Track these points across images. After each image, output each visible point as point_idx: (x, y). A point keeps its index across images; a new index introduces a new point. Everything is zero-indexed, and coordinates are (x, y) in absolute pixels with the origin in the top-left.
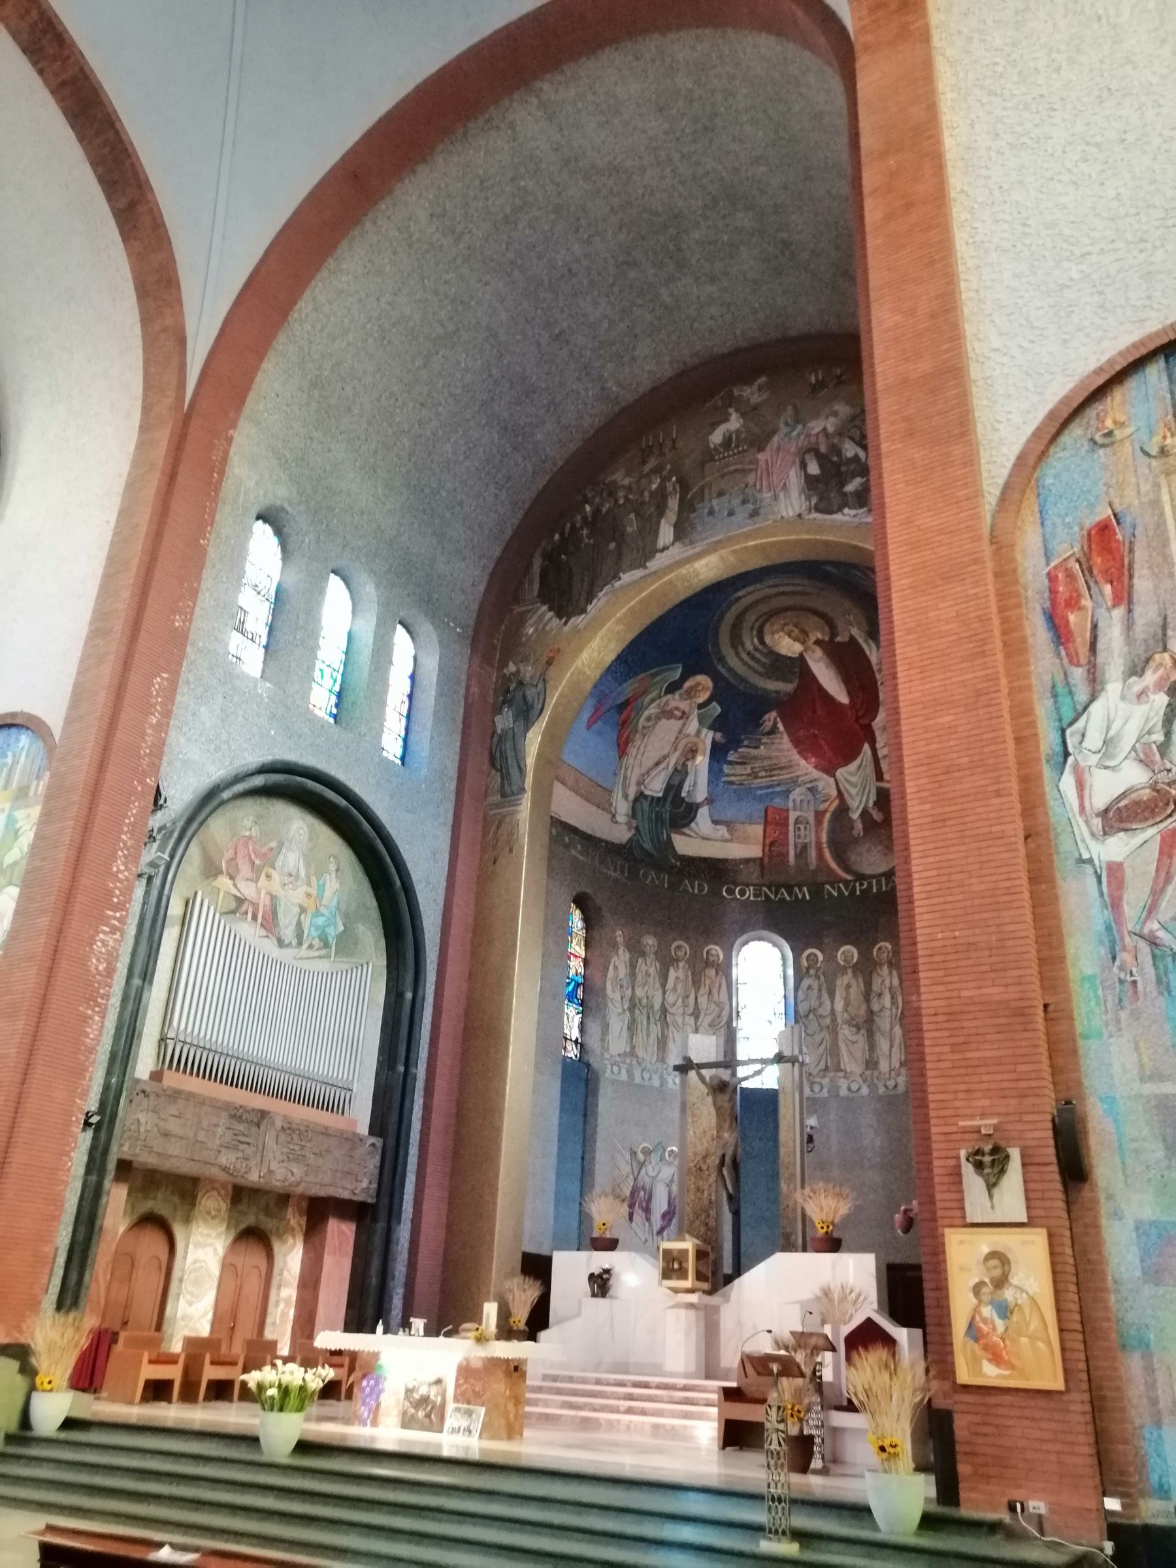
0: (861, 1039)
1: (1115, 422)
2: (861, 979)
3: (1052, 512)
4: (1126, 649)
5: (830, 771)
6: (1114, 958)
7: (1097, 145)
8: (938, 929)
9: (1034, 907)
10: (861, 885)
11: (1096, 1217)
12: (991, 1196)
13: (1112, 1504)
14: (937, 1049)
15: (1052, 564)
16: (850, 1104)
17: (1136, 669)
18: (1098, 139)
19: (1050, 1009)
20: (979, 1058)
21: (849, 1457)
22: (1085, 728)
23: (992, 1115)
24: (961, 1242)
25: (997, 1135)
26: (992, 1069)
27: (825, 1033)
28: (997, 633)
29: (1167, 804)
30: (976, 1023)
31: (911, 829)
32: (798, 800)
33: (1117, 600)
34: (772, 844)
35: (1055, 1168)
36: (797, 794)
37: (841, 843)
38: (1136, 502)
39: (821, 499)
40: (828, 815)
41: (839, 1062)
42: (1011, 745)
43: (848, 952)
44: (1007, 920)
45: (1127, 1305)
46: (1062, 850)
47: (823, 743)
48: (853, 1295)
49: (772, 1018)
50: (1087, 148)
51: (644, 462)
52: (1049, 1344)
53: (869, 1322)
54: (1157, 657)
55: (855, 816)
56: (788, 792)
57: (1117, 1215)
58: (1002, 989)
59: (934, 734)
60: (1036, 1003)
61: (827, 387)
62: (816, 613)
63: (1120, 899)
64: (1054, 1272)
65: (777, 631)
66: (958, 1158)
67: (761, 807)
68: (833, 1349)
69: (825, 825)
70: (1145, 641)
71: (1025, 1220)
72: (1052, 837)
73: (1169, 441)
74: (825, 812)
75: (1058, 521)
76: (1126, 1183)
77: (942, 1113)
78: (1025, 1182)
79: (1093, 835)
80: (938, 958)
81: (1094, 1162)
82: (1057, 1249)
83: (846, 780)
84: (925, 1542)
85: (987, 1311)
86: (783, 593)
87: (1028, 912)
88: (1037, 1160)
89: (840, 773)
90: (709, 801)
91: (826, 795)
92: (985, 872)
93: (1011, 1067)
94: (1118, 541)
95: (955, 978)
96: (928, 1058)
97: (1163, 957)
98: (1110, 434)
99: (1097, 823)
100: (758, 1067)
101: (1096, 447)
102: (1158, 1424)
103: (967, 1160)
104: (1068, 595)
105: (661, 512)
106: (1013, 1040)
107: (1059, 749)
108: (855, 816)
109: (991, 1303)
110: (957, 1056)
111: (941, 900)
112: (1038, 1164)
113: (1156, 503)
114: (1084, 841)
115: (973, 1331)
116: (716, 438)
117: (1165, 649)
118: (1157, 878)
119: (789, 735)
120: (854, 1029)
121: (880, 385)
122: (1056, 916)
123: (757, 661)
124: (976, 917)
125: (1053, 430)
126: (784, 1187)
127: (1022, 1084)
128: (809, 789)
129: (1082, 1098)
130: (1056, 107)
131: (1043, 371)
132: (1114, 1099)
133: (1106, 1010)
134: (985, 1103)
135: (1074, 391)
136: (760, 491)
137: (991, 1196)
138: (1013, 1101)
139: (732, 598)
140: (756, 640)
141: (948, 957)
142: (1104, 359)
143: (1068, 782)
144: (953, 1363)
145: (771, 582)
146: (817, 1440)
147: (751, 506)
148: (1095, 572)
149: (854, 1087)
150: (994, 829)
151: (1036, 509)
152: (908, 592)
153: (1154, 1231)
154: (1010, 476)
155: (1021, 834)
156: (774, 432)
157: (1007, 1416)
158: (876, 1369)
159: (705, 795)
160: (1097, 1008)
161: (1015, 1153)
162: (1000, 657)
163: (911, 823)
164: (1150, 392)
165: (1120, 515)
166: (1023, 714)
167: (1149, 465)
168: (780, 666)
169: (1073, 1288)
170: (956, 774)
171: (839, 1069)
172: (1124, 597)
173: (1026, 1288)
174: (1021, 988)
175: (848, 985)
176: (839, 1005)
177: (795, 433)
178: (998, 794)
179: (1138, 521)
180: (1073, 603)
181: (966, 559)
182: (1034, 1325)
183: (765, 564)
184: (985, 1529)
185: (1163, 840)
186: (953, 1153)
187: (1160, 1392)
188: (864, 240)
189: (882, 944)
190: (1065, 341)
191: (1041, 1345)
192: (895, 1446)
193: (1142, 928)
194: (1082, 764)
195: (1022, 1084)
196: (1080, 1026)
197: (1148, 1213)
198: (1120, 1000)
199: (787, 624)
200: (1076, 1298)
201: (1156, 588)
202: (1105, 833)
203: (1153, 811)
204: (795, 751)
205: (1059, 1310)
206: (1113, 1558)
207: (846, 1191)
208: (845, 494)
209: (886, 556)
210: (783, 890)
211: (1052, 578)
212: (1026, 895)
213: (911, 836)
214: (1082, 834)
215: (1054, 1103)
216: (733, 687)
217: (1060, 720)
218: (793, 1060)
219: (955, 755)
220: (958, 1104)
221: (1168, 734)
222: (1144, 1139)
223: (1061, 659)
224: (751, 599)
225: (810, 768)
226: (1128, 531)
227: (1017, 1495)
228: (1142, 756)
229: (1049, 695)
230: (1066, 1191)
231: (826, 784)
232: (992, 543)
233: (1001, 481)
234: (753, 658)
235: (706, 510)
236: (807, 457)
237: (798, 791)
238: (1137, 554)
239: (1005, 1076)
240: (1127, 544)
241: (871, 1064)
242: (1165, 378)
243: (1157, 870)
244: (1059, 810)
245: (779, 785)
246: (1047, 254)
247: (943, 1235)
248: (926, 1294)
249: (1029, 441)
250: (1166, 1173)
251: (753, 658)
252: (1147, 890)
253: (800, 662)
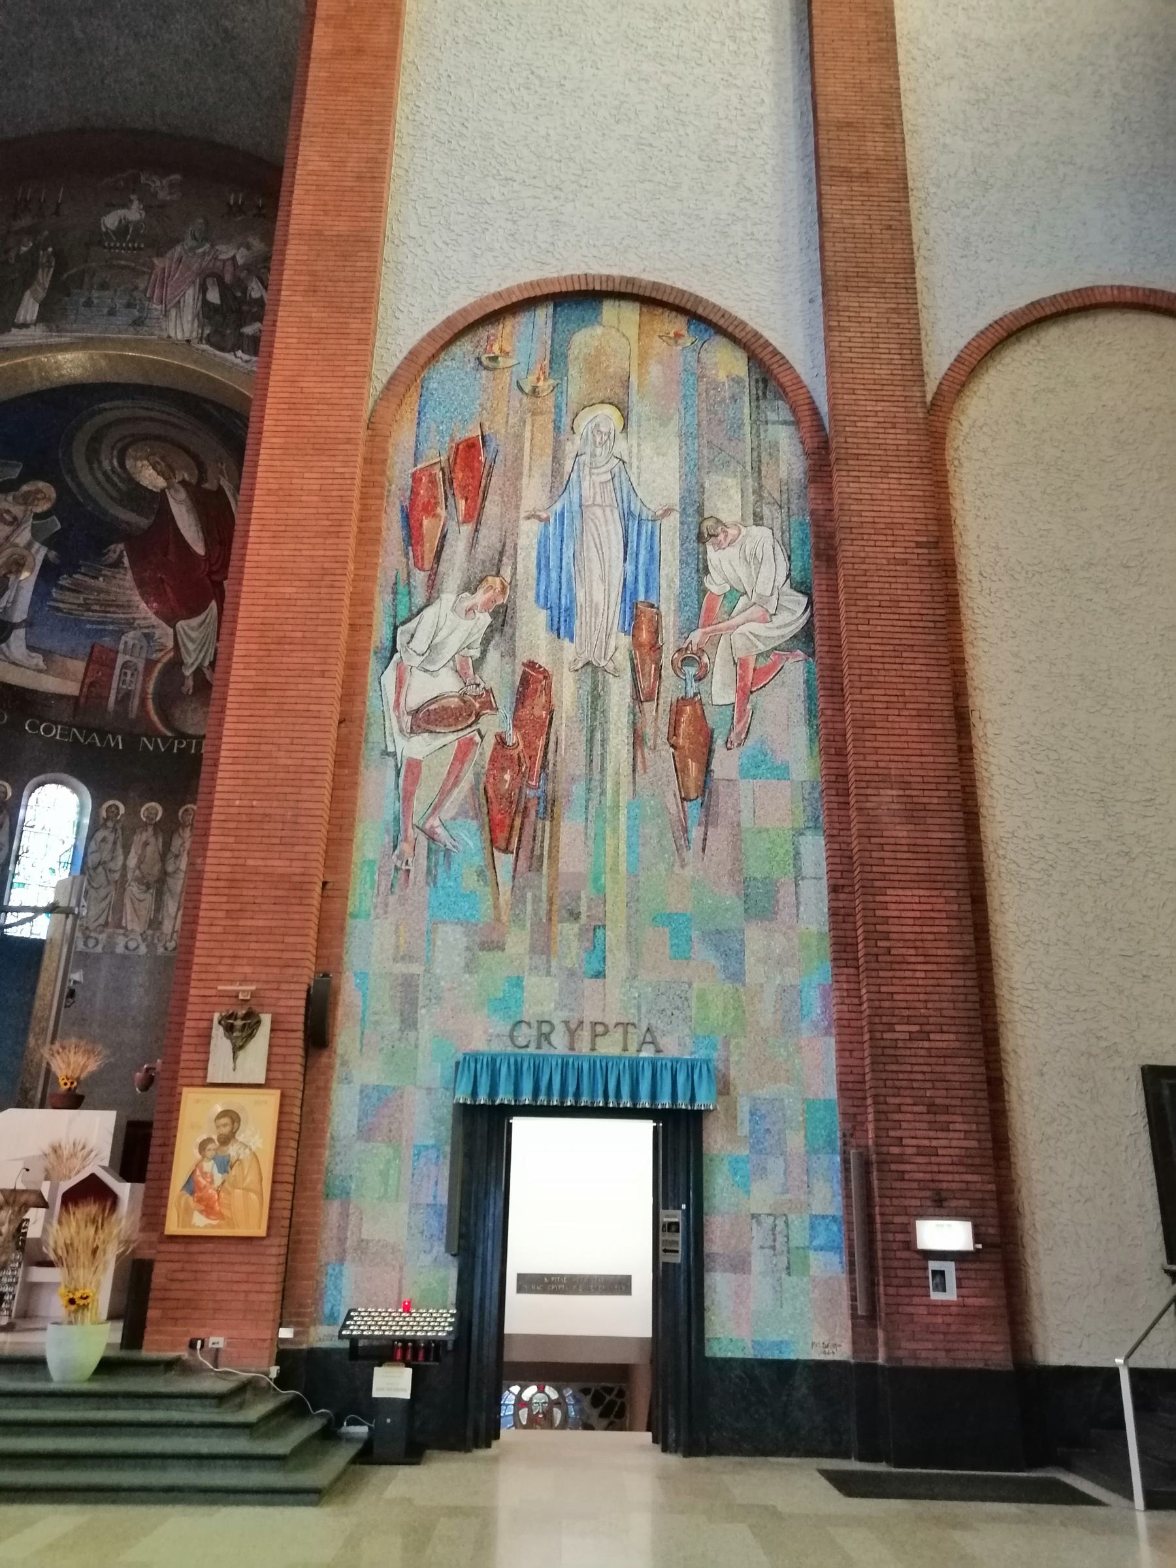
0: (149, 898)
1: (501, 350)
2: (161, 840)
3: (429, 415)
4: (465, 565)
5: (171, 621)
6: (395, 847)
7: (539, 77)
8: (237, 796)
10: (180, 743)
11: (328, 1081)
12: (235, 1058)
15: (419, 466)
16: (125, 960)
17: (470, 587)
18: (542, 73)
19: (328, 886)
23: (251, 982)
24: (198, 1101)
25: (254, 1001)
26: (261, 938)
27: (112, 887)
28: (354, 517)
29: (470, 715)
31: (230, 692)
32: (131, 643)
34: (92, 684)
35: (301, 1035)
36: (130, 637)
39: (215, 332)
40: (159, 666)
41: (120, 919)
42: (344, 630)
43: (153, 809)
45: (338, 1159)
46: (370, 739)
47: (168, 589)
49: (56, 866)
50: (531, 77)
51: (15, 216)
53: (93, 1177)
54: (490, 578)
55: (188, 672)
56: (122, 633)
57: (347, 1080)
58: (287, 863)
60: (315, 879)
62: (195, 457)
63: (412, 794)
64: (280, 1130)
65: (141, 459)
67: (89, 642)
68: (45, 1205)
69: (155, 674)
70: (483, 562)
71: (263, 1082)
72: (364, 726)
73: (541, 383)
74: (158, 661)
75: (434, 426)
77: (203, 976)
78: (270, 1046)
79: (401, 730)
80: (232, 825)
81: (337, 1031)
84: (96, 1386)
85: (209, 1166)
86: (151, 419)
87: (327, 792)
88: (286, 1026)
89: (181, 624)
90: (28, 624)
91: (162, 644)
92: (293, 748)
94: (480, 462)
95: (244, 847)
96: (201, 921)
98: (494, 359)
99: (408, 719)
100: (31, 914)
102: (341, 1261)
103: (220, 1023)
105: (27, 282)
106: (287, 912)
107: (388, 644)
108: (188, 672)
110: (229, 922)
111: (248, 768)
113: (519, 437)
114: (392, 735)
115: (191, 1186)
116: (111, 221)
117: (498, 574)
118: (447, 779)
120: (144, 888)
121: (293, 228)
122: (353, 801)
123: (114, 485)
124: (278, 789)
125: (447, 337)
126: (32, 1041)
128: (146, 635)
130: (513, 22)
134: (248, 969)
135: (473, 306)
136: (150, 299)
137: (235, 1058)
138: (276, 970)
139: (96, 407)
140: (115, 463)
141: (241, 825)
142: (505, 286)
143: (389, 678)
144: (165, 1216)
145: (144, 404)
146: (7, 1298)
148: (455, 485)
149: (132, 945)
150: (312, 707)
152: (277, 452)
153: (376, 1094)
155: (336, 717)
156: (178, 241)
158: (82, 1225)
159: (25, 617)
161: (266, 1019)
162: (352, 541)
163: (231, 686)
164: (536, 333)
165: (487, 438)
166: (362, 603)
167: (521, 401)
168: (138, 495)
169: (294, 1144)
170: (287, 647)
171: (119, 926)
172: (475, 515)
174: (305, 864)
175: (145, 843)
176: (132, 861)
177: (201, 250)
178: (323, 673)
179: (500, 448)
180: (429, 509)
181: (340, 436)
182: (251, 1178)
183: (140, 381)
184: (162, 1367)
185: (459, 746)
186: (206, 1016)
187: (349, 1234)
188: (307, 66)
189: (189, 806)
190: (475, 256)
191: (253, 1196)
192: (86, 1298)
194: (406, 663)
197: (373, 1079)
199: (154, 454)
200: (294, 1153)
201: (502, 515)
202: (412, 731)
205: (276, 1164)
207: (100, 1047)
208: (241, 335)
211: (416, 478)
213: (230, 699)
217: (395, 617)
218: (67, 912)
219: (290, 628)
220: (222, 968)
221: (484, 653)
223: (408, 559)
225: (150, 614)
226: (490, 456)
228: (458, 668)
229: (390, 590)
230: (307, 1056)
231: (164, 634)
233: (391, 370)
235: (83, 300)
236: (209, 281)
237: (131, 634)
239: (272, 946)
240: (487, 467)
241: (155, 924)
242: (550, 324)
244: (377, 702)
245: (112, 623)
246: (476, 163)
249: (423, 340)
250: (397, 1043)
253: (159, 500)
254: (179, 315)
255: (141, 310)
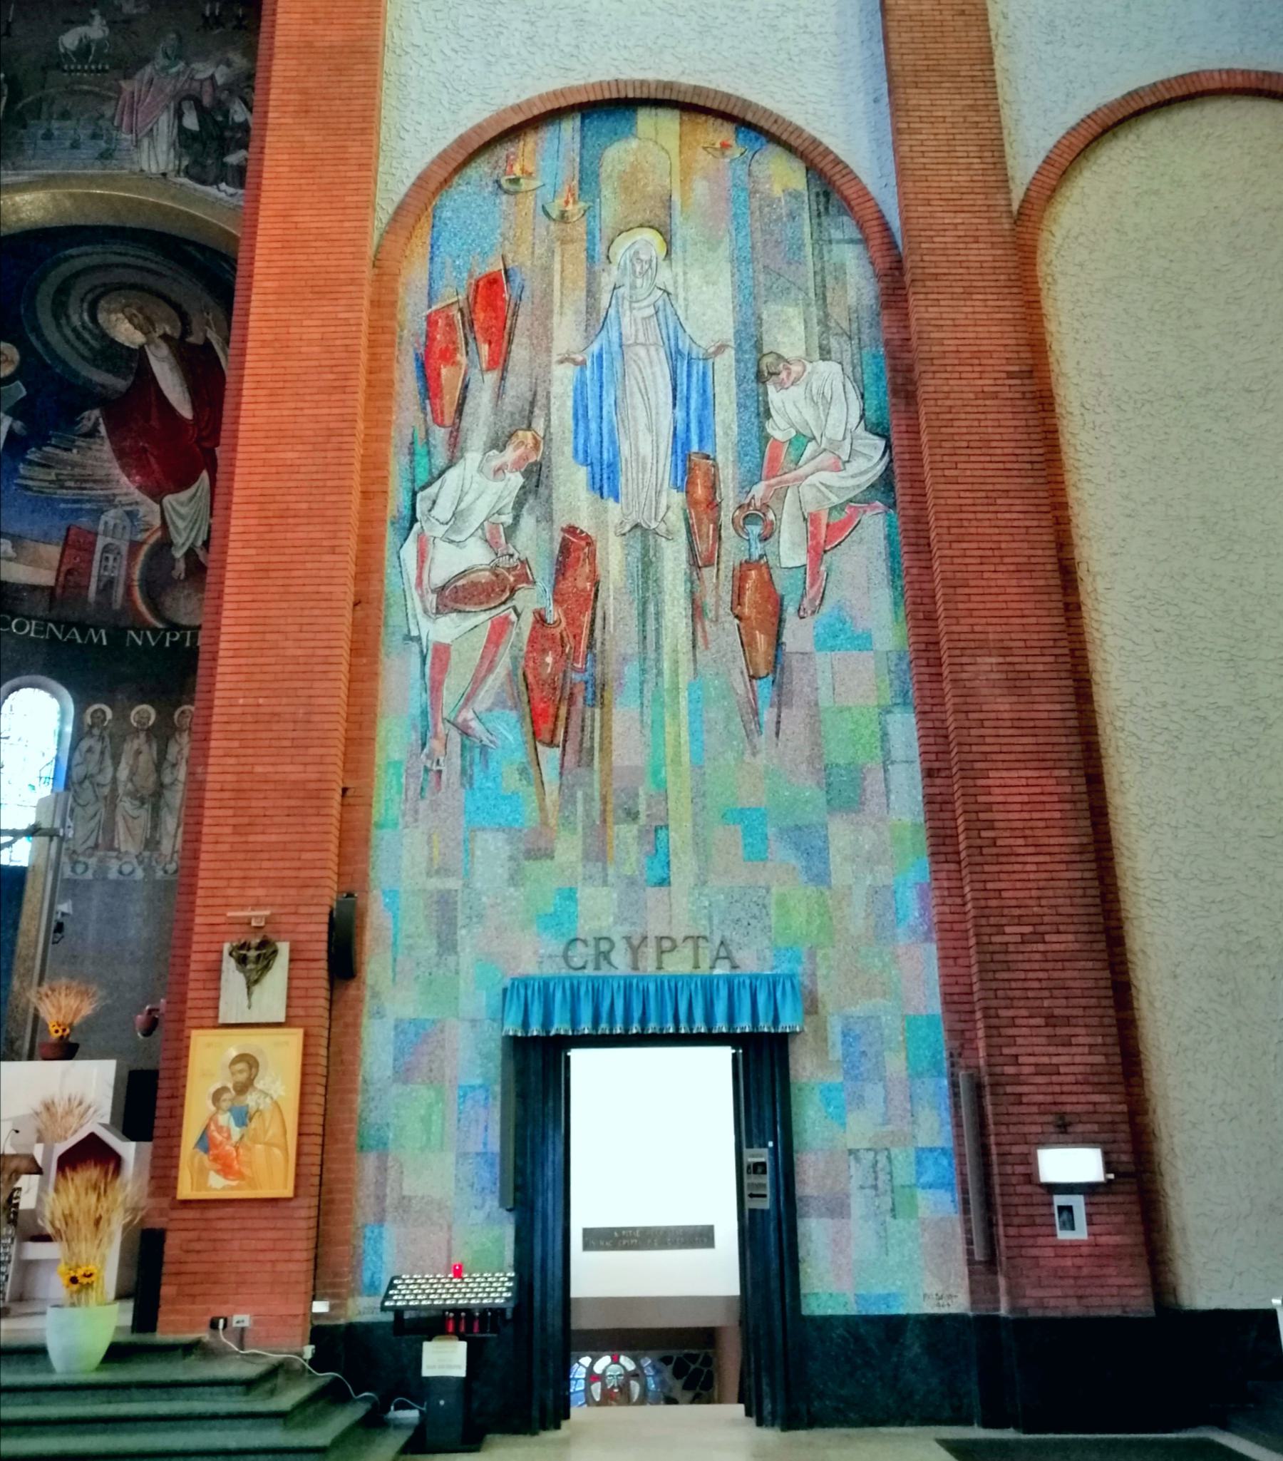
0: (144, 814)
1: (523, 170)
5: (157, 496)
6: (424, 745)
8: (240, 693)
9: (350, 681)
10: (173, 635)
11: (357, 1016)
12: (249, 994)
13: (320, 1307)
14: (216, 830)
15: (434, 308)
16: (120, 887)
17: (498, 443)
19: (349, 793)
20: (262, 843)
21: (40, 1294)
22: (437, 496)
23: (265, 906)
24: (209, 1045)
26: (274, 855)
27: (101, 804)
28: (362, 369)
29: (503, 591)
30: (262, 803)
31: (228, 575)
32: (111, 523)
33: (492, 364)
34: (69, 572)
35: (324, 964)
36: (110, 516)
37: (157, 585)
38: (528, 263)
39: (195, 162)
40: (146, 548)
41: (112, 840)
42: (356, 498)
43: (145, 713)
44: (318, 692)
45: (372, 1105)
46: (391, 623)
47: (152, 460)
48: (82, 1108)
49: (36, 782)
52: (286, 1150)
53: (92, 1137)
54: (520, 433)
55: (179, 554)
57: (379, 1014)
58: (301, 768)
59: (274, 470)
60: (334, 786)
61: (223, 25)
62: (176, 307)
63: (441, 683)
64: (304, 1074)
65: (115, 311)
66: (221, 952)
67: (64, 524)
68: (39, 1171)
70: (512, 414)
71: (282, 1019)
72: (383, 607)
73: (570, 207)
75: (449, 261)
76: (394, 980)
77: (210, 901)
79: (425, 611)
81: (366, 958)
82: (311, 1050)
83: (174, 509)
85: (225, 1119)
87: (343, 685)
89: (169, 500)
93: (296, 855)
94: (503, 300)
95: (250, 751)
96: (205, 839)
97: (471, 749)
98: (515, 181)
99: (432, 598)
101: (500, 192)
102: (381, 1222)
103: (231, 954)
104: (444, 345)
106: (303, 825)
107: (406, 512)
108: (179, 554)
109: (230, 1110)
110: (237, 839)
111: (251, 661)
112: (308, 960)
113: (547, 270)
114: (415, 616)
115: (205, 1143)
116: (70, 40)
117: (529, 428)
118: (480, 665)
119: (112, 442)
120: (137, 803)
121: (279, 41)
122: (373, 694)
123: (86, 343)
124: (287, 684)
125: (460, 159)
126: (16, 983)
127: (304, 874)
129: (366, 892)
131: (461, 89)
132: (397, 892)
133: (406, 800)
134: (260, 892)
135: (489, 121)
136: (119, 128)
137: (249, 994)
138: (293, 892)
139: (61, 255)
142: (524, 97)
144: (176, 1178)
145: (116, 248)
147: (103, 144)
148: (476, 327)
149: (127, 869)
150: (322, 589)
151: (428, 241)
153: (412, 1029)
154: (407, 195)
155: (351, 599)
156: (147, 60)
157: (226, 1230)
158: (82, 1191)
160: (397, 798)
161: (284, 948)
162: (361, 397)
163: (229, 567)
164: (562, 149)
165: (511, 272)
166: (375, 467)
167: (548, 228)
169: (321, 1090)
170: (291, 521)
172: (500, 361)
173: (272, 1092)
174: (322, 768)
175: (139, 754)
176: (123, 773)
177: (174, 70)
178: (333, 550)
179: (527, 283)
180: (448, 356)
181: (342, 276)
184: (180, 1352)
185: (493, 627)
186: (215, 947)
190: (489, 63)
191: (277, 1151)
192: (90, 1275)
193: (457, 716)
194: (428, 533)
195: (304, 874)
196: (377, 813)
197: (408, 1012)
198: (422, 789)
200: (322, 1100)
201: (532, 360)
202: (438, 612)
203: (489, 595)
204: (116, 464)
205: (301, 1114)
206: (311, 1362)
207: (94, 988)
208: (224, 165)
209: (252, 248)
210: (74, 630)
211: (431, 321)
212: (344, 668)
213: (228, 582)
214: (414, 609)
215: (335, 896)
216: (47, 367)
217: (413, 481)
218: (51, 834)
219: (293, 498)
220: (230, 892)
221: (517, 518)
222: (419, 936)
223: (426, 415)
224: (87, 261)
226: (516, 292)
227: (221, 1310)
231: (149, 510)
232: (374, 266)
233: (397, 199)
234: (79, 336)
235: (41, 132)
237: (112, 512)
238: (520, 319)
239: (288, 864)
240: (512, 305)
241: (152, 843)
242: (578, 138)
243: (482, 658)
245: (89, 501)
247: (189, 1037)
248: (159, 1103)
249: (433, 162)
250: (435, 969)
251: (79, 336)
252: (469, 677)
253: (140, 355)
254: (152, 145)
255: (109, 141)
